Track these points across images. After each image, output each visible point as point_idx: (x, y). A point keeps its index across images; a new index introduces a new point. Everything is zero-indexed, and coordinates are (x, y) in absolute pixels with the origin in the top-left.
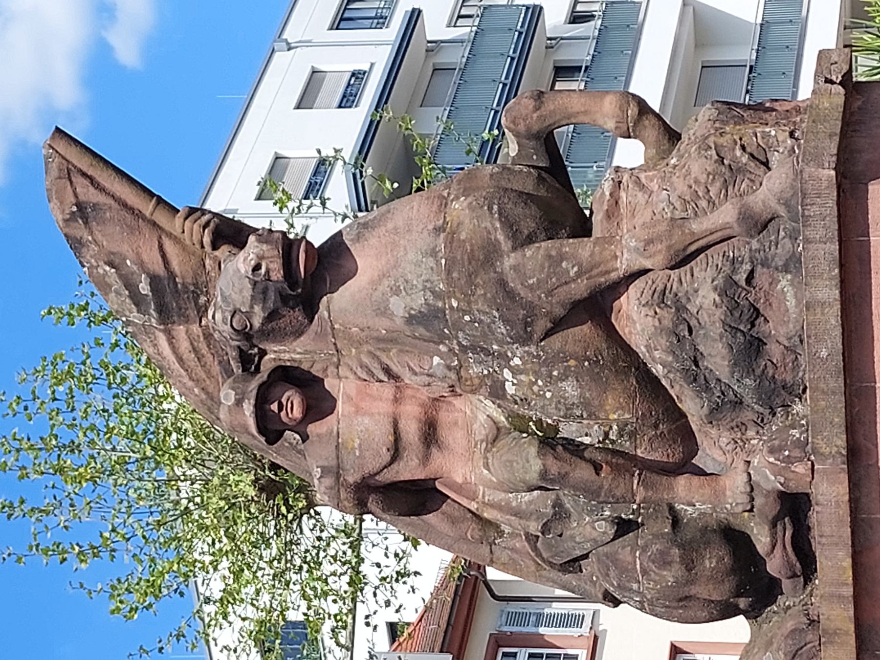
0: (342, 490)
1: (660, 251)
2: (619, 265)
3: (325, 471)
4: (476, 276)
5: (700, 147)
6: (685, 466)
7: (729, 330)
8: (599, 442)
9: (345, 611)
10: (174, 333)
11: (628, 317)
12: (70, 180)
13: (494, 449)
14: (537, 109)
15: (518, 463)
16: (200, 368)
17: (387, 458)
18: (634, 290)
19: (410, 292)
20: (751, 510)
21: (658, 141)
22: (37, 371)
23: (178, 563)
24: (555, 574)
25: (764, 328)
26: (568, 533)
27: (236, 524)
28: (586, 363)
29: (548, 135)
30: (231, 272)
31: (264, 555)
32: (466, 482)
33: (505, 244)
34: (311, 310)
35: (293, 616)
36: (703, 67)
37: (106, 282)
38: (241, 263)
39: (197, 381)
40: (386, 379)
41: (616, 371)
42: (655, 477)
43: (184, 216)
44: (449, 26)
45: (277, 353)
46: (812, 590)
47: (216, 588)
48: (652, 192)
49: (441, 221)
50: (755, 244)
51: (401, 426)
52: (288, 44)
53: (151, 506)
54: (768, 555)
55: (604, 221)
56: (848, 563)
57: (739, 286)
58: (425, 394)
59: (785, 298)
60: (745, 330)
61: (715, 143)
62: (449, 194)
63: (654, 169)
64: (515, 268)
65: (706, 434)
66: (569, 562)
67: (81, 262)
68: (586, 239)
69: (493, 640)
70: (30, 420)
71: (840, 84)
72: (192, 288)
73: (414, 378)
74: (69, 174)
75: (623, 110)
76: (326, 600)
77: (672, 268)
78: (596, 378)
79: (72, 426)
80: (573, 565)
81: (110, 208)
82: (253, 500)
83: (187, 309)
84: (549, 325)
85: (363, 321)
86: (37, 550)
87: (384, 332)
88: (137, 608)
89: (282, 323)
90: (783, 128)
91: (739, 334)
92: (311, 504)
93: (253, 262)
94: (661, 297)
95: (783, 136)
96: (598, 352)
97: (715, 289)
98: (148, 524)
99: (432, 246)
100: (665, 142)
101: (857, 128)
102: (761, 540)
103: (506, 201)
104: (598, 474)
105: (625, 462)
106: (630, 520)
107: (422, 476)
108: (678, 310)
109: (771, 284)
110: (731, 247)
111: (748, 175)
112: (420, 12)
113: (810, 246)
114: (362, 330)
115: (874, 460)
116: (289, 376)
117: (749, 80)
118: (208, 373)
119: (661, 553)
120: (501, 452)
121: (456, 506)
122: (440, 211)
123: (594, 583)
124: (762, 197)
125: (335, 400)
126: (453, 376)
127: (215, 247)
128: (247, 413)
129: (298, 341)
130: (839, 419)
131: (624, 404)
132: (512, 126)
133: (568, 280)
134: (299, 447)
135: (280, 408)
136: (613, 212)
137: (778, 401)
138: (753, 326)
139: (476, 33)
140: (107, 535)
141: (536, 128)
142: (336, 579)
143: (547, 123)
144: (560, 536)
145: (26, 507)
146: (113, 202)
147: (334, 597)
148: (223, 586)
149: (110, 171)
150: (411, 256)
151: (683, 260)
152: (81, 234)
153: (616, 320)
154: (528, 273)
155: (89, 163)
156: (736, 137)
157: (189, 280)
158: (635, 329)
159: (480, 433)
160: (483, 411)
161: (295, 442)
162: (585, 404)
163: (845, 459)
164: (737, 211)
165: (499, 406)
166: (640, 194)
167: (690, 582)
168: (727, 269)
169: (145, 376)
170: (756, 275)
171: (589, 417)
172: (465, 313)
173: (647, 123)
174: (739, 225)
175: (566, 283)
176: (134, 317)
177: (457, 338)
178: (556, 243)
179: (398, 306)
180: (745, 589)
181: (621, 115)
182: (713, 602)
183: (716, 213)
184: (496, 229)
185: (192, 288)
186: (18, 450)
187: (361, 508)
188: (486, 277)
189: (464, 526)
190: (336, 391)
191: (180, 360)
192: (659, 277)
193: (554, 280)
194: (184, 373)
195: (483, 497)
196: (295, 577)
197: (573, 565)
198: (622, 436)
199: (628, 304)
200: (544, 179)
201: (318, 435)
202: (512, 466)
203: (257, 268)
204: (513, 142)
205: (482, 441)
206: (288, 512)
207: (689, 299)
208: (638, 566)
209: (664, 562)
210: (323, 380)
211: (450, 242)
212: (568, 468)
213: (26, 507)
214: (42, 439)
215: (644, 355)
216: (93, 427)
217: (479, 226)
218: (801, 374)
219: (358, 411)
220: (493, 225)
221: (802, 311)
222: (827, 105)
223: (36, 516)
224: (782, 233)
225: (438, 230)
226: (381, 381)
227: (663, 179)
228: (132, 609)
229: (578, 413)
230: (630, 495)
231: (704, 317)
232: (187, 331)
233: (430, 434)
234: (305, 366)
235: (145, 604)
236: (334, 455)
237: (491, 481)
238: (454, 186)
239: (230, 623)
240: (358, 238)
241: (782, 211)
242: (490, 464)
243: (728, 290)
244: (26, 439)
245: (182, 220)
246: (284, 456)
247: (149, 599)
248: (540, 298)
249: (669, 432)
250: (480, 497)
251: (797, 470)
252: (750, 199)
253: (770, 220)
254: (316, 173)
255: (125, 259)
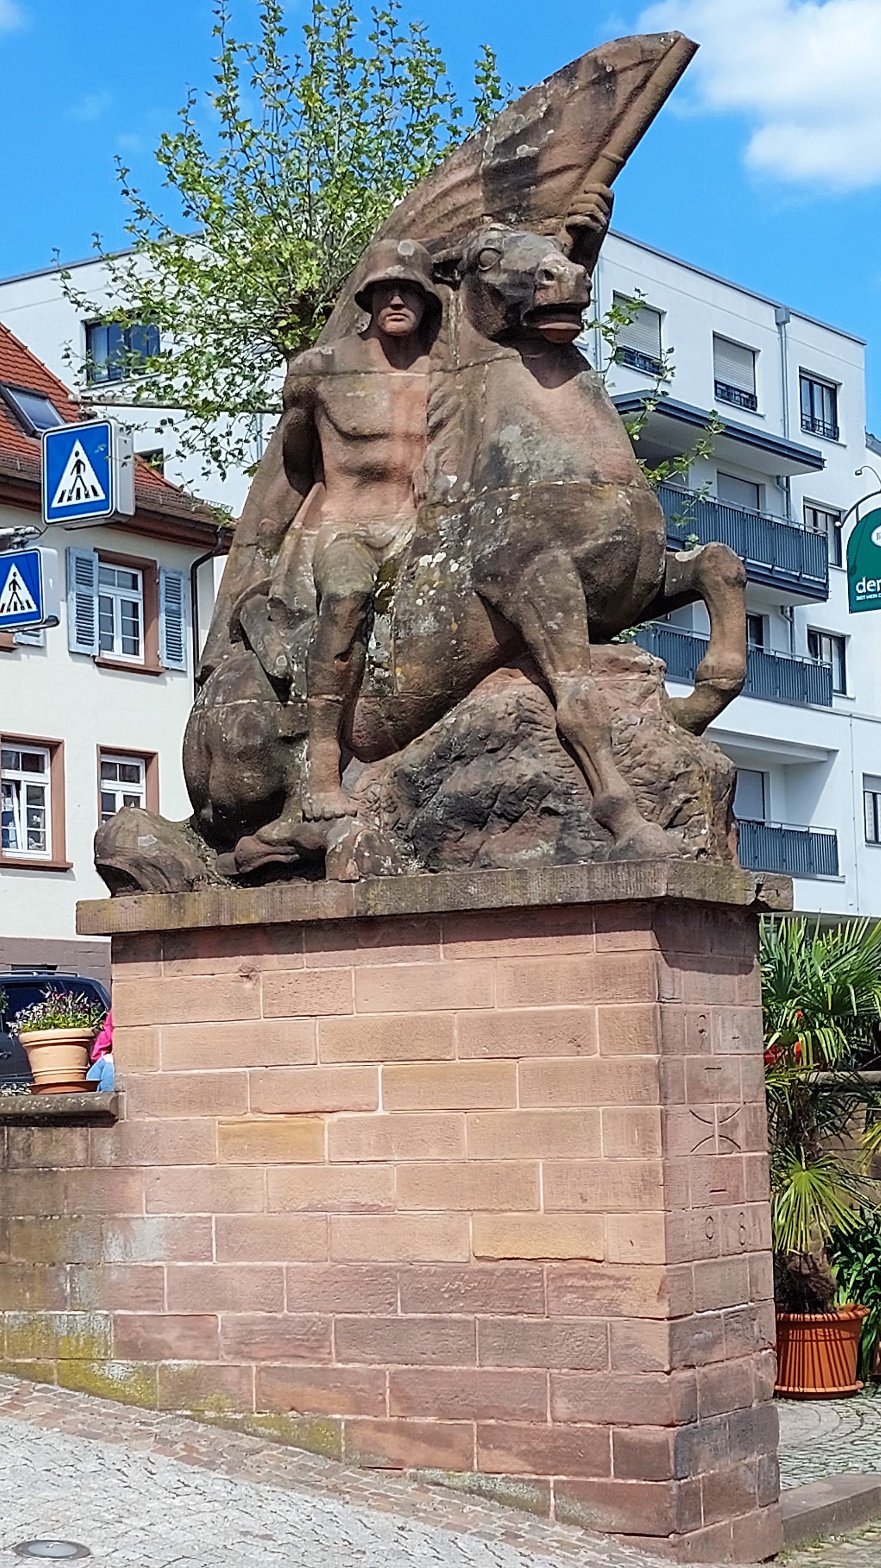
0: (309, 379)
1: (576, 716)
2: (561, 673)
3: (329, 359)
4: (544, 519)
5: (688, 755)
6: (349, 750)
7: (494, 791)
8: (371, 658)
9: (176, 396)
10: (474, 186)
11: (505, 686)
12: (637, 65)
13: (359, 545)
14: (727, 580)
15: (345, 570)
16: (436, 216)
17: (346, 427)
18: (534, 690)
19: (526, 447)
20: (305, 818)
21: (693, 711)
22: (424, 44)
23: (220, 209)
24: (228, 614)
25: (497, 828)
26: (273, 627)
27: (266, 271)
28: (454, 642)
29: (699, 593)
30: (544, 247)
31: (232, 304)
32: (322, 515)
33: (579, 550)
34: (504, 337)
35: (167, 341)
36: (762, 773)
37: (528, 108)
38: (553, 257)
39: (422, 214)
40: (430, 424)
41: (447, 674)
42: (336, 718)
43: (603, 192)
44: (805, 499)
45: (455, 302)
46: (224, 884)
47: (195, 252)
48: (639, 707)
49: (603, 479)
50: (585, 816)
51: (381, 441)
52: (784, 323)
53: (281, 176)
54: (259, 838)
55: (606, 657)
56: (254, 919)
57: (540, 800)
58: (415, 467)
59: (529, 848)
60: (495, 808)
61: (691, 772)
62: (633, 487)
63: (663, 708)
64: (555, 561)
65: (383, 771)
66: (244, 631)
67: (549, 78)
68: (587, 637)
69: (150, 564)
70: (371, 39)
71: (756, 900)
72: (524, 204)
73: (433, 454)
74: (647, 61)
75: (727, 673)
76: (186, 375)
77: (558, 730)
78: (439, 652)
79: (364, 82)
80: (239, 633)
81: (611, 109)
82: (291, 290)
83: (501, 199)
84: (494, 600)
85: (492, 396)
86: (229, 49)
87: (482, 420)
88: (170, 164)
89: (489, 305)
90: (709, 842)
91: (490, 802)
92: (289, 355)
93: (555, 270)
94: (526, 720)
95: (701, 842)
96: (466, 654)
97: (537, 776)
98: (261, 172)
99: (577, 470)
100: (692, 720)
101: (710, 918)
102: (274, 830)
103: (627, 549)
104: (337, 657)
105: (350, 684)
106: (290, 692)
107: (327, 466)
108: (514, 737)
109: (544, 833)
110: (581, 791)
111: (659, 807)
112: (821, 468)
113: (585, 872)
114: (484, 395)
115: (362, 944)
116: (431, 315)
117: (749, 822)
118: (432, 226)
119: (256, 725)
120: (356, 552)
121: (297, 506)
122: (614, 478)
123: (221, 657)
124: (636, 821)
125: (406, 367)
126: (436, 498)
127: (570, 228)
128: (389, 270)
129: (470, 325)
130: (404, 907)
131: (412, 683)
132: (708, 553)
133: (543, 619)
134: (353, 330)
135: (397, 307)
136: (614, 664)
137: (421, 844)
138: (500, 816)
139: (798, 530)
140: (248, 127)
141: (706, 580)
142: (210, 385)
143: (710, 591)
144: (269, 619)
145: (275, 36)
146: (617, 112)
147: (190, 384)
148: (197, 260)
149: (651, 108)
150: (565, 447)
151: (568, 741)
152: (581, 77)
153: (502, 673)
154: (549, 576)
155: (660, 83)
156: (698, 794)
157: (533, 201)
158: (493, 693)
159: (375, 529)
160: (399, 532)
161: (359, 325)
162: (411, 642)
163: (363, 914)
164: (620, 796)
165: (405, 549)
166: (636, 694)
167: (227, 756)
168: (558, 787)
169: (423, 165)
170: (553, 818)
171: (397, 647)
172: (505, 508)
173: (713, 699)
174: (605, 799)
175: (540, 617)
176: (491, 141)
177: (478, 501)
178: (583, 606)
179: (510, 435)
180: (222, 815)
181: (722, 670)
182: (207, 781)
183: (618, 774)
184: (596, 539)
185: (524, 204)
186: (337, 24)
187: (291, 400)
188: (544, 530)
189: (274, 514)
190: (416, 369)
191: (445, 194)
192: (548, 718)
193: (543, 604)
194: (431, 198)
195: (307, 535)
196: (210, 340)
197: (239, 633)
198: (378, 682)
199: (519, 685)
200: (650, 591)
201: (367, 351)
202: (343, 564)
203: (549, 275)
204: (690, 555)
205: (367, 532)
206: (280, 329)
207: (526, 749)
208: (240, 702)
209: (248, 728)
210: (427, 353)
211: (581, 490)
212: (342, 623)
213: (275, 36)
214: (351, 51)
215: (465, 704)
216: (363, 106)
217: (599, 521)
218: (449, 866)
219: (395, 394)
220: (601, 536)
221: (516, 866)
222: (734, 886)
223: (266, 47)
224: (597, 843)
225: (594, 476)
226: (428, 419)
227: (653, 718)
228: (169, 158)
229: (401, 634)
230: (315, 691)
231: (507, 765)
232: (476, 200)
233: (373, 475)
234: (442, 334)
235: (175, 174)
236: (346, 368)
237: (325, 542)
238: (642, 493)
239: (157, 268)
240: (584, 388)
241: (621, 843)
242: (343, 541)
243: (537, 789)
244: (349, 33)
245: (599, 190)
246: (343, 314)
247: (180, 178)
248: (524, 589)
249: (385, 732)
250: (307, 532)
251: (349, 865)
252: (633, 809)
253: (611, 831)
254: (646, 359)
255: (554, 128)
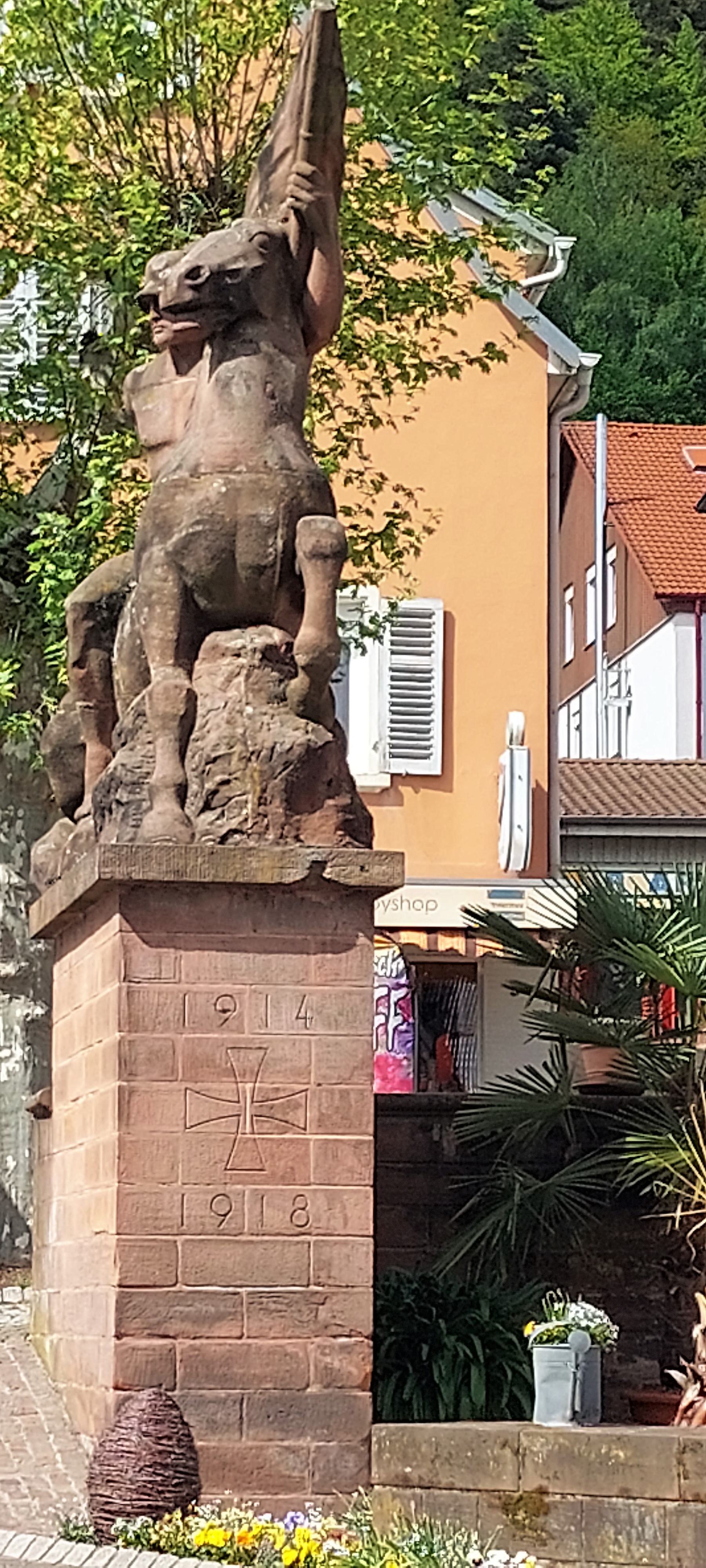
51: (166, 449)
62: (240, 472)
